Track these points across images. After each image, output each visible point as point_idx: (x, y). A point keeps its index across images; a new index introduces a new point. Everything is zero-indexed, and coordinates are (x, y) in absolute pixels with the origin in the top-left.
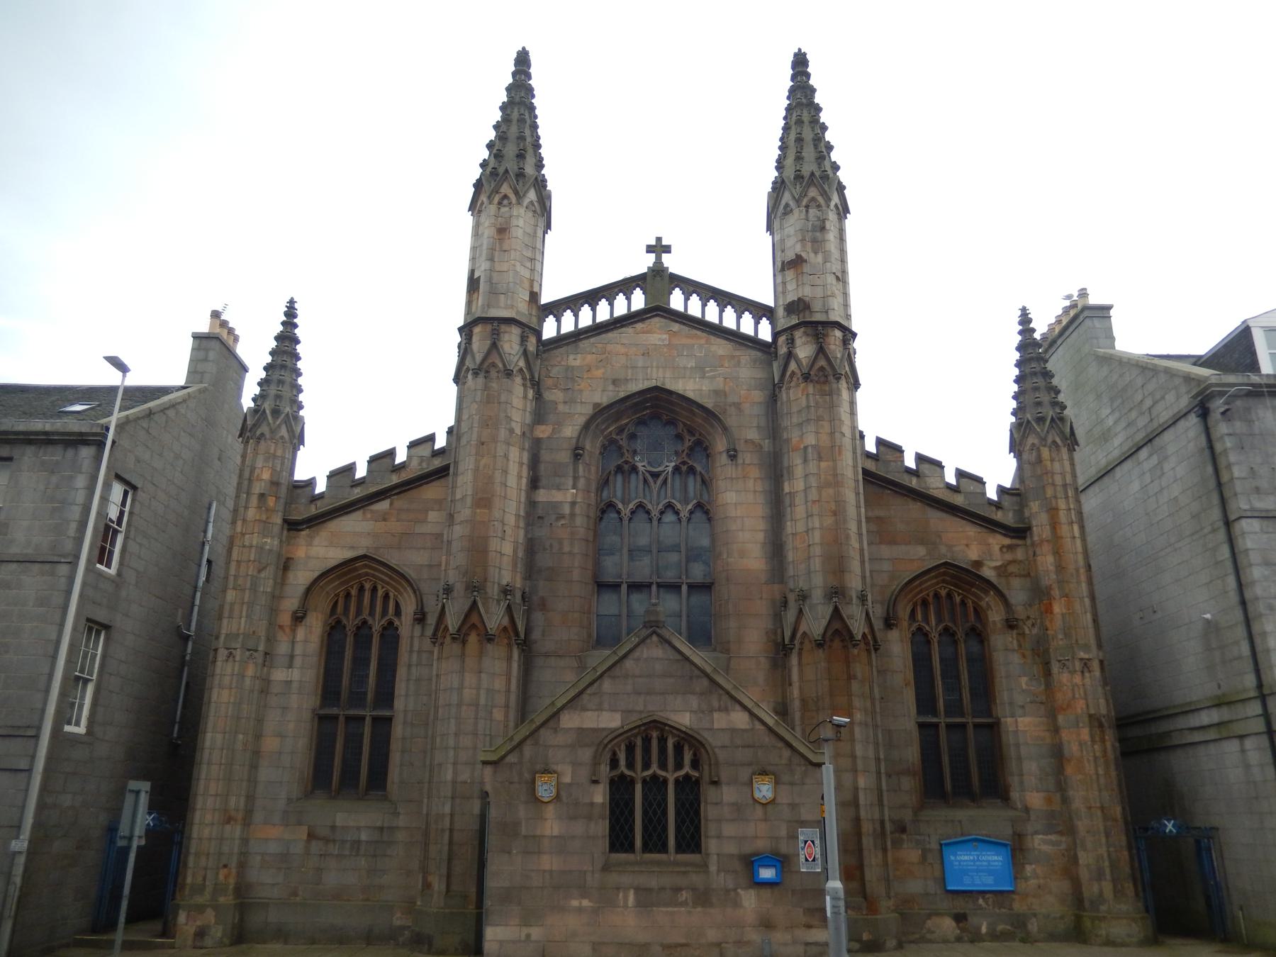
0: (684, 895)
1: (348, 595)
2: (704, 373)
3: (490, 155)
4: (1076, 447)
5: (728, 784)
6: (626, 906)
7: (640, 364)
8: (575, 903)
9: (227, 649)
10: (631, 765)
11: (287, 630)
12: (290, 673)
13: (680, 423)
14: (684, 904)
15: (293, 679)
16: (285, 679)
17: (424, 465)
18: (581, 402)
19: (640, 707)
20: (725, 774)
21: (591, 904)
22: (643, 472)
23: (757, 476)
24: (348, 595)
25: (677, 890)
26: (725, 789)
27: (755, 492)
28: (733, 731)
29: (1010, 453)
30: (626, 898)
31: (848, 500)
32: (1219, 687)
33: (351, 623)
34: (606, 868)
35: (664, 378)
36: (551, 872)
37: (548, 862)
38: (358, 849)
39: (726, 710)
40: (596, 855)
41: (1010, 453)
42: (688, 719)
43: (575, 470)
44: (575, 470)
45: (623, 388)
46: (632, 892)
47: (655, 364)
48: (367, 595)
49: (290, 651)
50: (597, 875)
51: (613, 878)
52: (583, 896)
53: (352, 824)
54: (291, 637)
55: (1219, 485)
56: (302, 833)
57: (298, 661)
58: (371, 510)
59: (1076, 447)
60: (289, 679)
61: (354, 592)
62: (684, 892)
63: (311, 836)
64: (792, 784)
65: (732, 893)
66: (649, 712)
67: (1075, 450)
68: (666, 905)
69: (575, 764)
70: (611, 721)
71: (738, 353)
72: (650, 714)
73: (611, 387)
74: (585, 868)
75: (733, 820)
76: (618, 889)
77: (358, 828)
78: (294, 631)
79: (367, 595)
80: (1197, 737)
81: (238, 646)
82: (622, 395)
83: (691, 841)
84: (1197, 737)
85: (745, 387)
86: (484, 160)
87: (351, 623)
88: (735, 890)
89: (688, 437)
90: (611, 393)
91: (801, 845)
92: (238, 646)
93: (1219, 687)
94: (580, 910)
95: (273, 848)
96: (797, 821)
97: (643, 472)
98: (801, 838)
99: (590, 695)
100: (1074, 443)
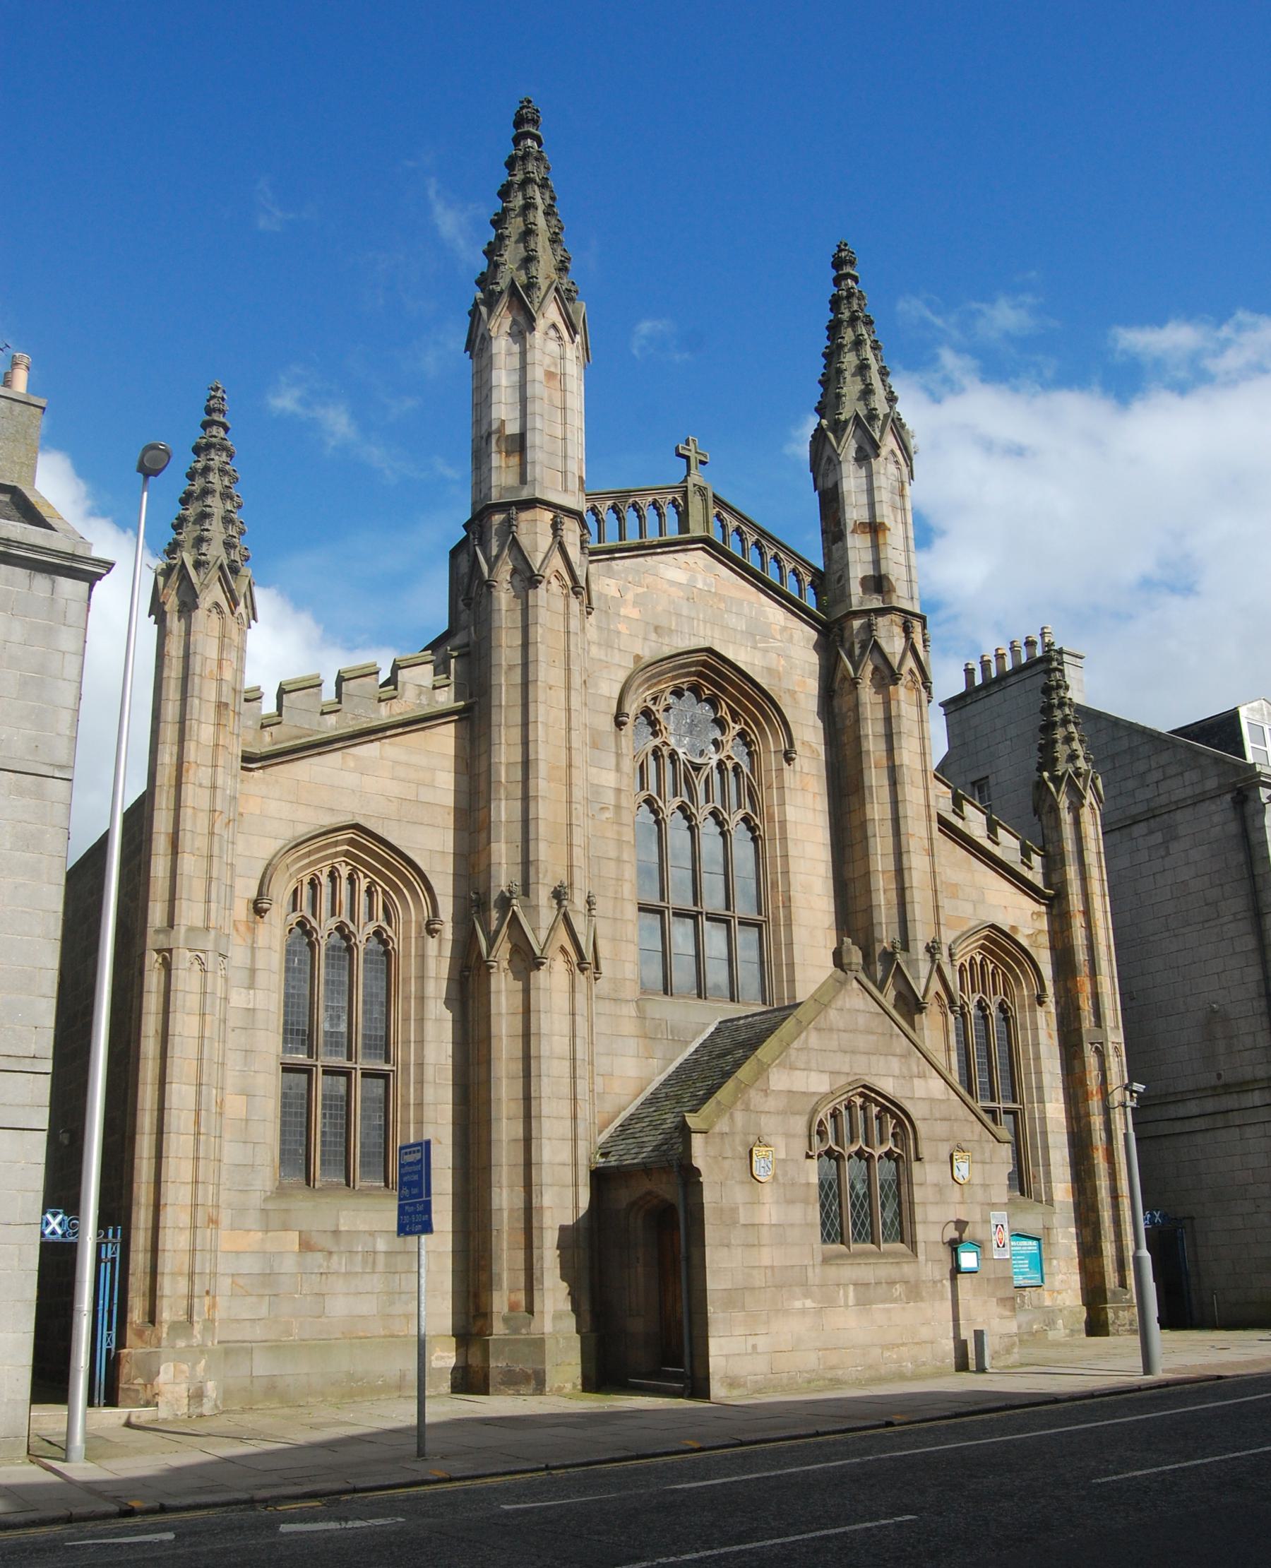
0: (898, 1289)
1: (314, 884)
2: (755, 642)
3: (489, 266)
4: (253, 622)
5: (930, 1162)
6: (847, 1306)
7: (685, 612)
8: (798, 1304)
9: (191, 950)
10: (838, 1141)
11: (242, 928)
12: (251, 997)
13: (723, 703)
14: (895, 1300)
15: (257, 1007)
16: (245, 1006)
17: (424, 700)
18: (620, 650)
19: (846, 1069)
20: (925, 1151)
21: (813, 1305)
22: (684, 763)
23: (816, 791)
24: (314, 884)
25: (892, 1283)
26: (927, 1166)
27: (814, 810)
28: (932, 1100)
29: (149, 616)
30: (846, 1297)
31: (910, 832)
32: (1219, 1076)
33: (325, 926)
34: (826, 1260)
35: (713, 637)
36: (772, 1267)
37: (767, 1257)
38: (374, 1263)
39: (922, 1076)
40: (815, 1246)
41: (149, 616)
42: (891, 1085)
43: (618, 745)
44: (618, 745)
45: (666, 640)
46: (851, 1288)
47: (701, 616)
48: (344, 885)
49: (249, 962)
50: (817, 1270)
51: (833, 1272)
52: (807, 1295)
53: (362, 1227)
54: (249, 941)
55: (1253, 876)
56: (291, 1240)
57: (261, 978)
58: (354, 755)
59: (253, 622)
60: (251, 1006)
61: (324, 879)
62: (898, 1286)
63: (306, 1246)
64: (983, 1163)
65: (939, 1285)
66: (856, 1074)
67: (250, 627)
68: (883, 1301)
69: (788, 1135)
70: (819, 1084)
71: (790, 625)
72: (858, 1077)
73: (653, 636)
74: (806, 1262)
75: (937, 1203)
76: (838, 1285)
77: (372, 1234)
78: (252, 931)
79: (344, 885)
80: (1178, 1127)
81: (210, 946)
82: (667, 651)
83: (903, 1229)
84: (1178, 1127)
85: (799, 672)
86: (482, 274)
87: (325, 926)
88: (941, 1281)
89: (732, 724)
90: (653, 644)
91: (993, 1229)
92: (210, 946)
93: (1219, 1076)
94: (804, 1311)
95: (250, 1265)
96: (989, 1204)
97: (684, 763)
98: (993, 1222)
99: (798, 1050)
100: (251, 617)
